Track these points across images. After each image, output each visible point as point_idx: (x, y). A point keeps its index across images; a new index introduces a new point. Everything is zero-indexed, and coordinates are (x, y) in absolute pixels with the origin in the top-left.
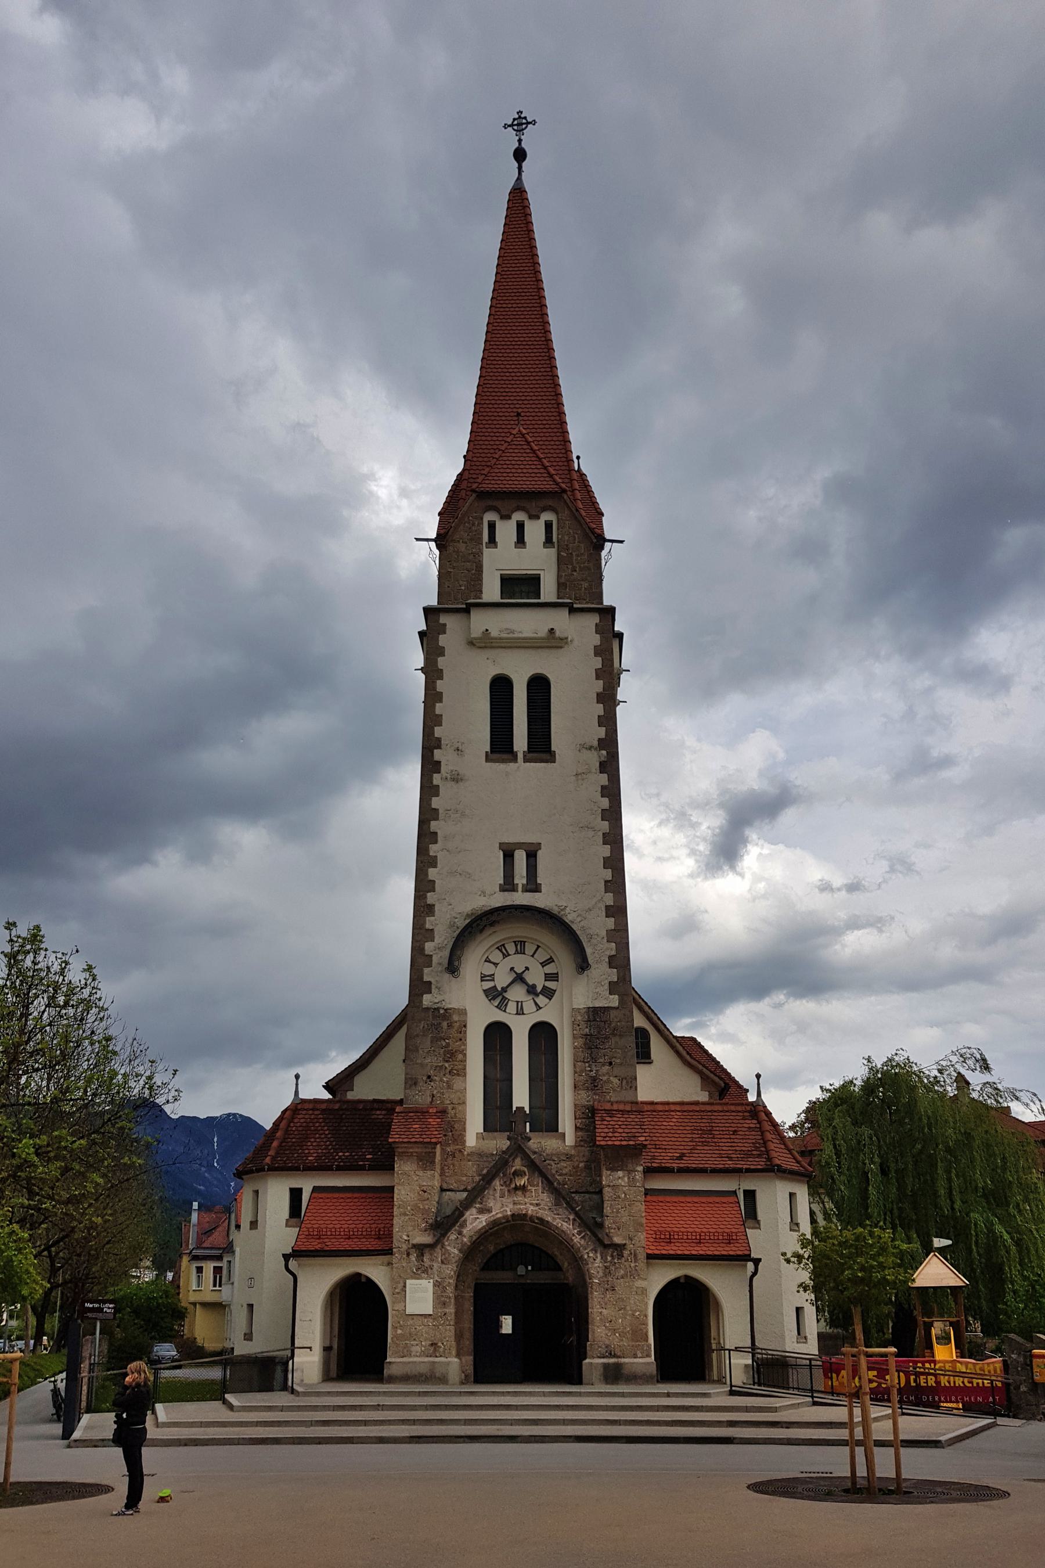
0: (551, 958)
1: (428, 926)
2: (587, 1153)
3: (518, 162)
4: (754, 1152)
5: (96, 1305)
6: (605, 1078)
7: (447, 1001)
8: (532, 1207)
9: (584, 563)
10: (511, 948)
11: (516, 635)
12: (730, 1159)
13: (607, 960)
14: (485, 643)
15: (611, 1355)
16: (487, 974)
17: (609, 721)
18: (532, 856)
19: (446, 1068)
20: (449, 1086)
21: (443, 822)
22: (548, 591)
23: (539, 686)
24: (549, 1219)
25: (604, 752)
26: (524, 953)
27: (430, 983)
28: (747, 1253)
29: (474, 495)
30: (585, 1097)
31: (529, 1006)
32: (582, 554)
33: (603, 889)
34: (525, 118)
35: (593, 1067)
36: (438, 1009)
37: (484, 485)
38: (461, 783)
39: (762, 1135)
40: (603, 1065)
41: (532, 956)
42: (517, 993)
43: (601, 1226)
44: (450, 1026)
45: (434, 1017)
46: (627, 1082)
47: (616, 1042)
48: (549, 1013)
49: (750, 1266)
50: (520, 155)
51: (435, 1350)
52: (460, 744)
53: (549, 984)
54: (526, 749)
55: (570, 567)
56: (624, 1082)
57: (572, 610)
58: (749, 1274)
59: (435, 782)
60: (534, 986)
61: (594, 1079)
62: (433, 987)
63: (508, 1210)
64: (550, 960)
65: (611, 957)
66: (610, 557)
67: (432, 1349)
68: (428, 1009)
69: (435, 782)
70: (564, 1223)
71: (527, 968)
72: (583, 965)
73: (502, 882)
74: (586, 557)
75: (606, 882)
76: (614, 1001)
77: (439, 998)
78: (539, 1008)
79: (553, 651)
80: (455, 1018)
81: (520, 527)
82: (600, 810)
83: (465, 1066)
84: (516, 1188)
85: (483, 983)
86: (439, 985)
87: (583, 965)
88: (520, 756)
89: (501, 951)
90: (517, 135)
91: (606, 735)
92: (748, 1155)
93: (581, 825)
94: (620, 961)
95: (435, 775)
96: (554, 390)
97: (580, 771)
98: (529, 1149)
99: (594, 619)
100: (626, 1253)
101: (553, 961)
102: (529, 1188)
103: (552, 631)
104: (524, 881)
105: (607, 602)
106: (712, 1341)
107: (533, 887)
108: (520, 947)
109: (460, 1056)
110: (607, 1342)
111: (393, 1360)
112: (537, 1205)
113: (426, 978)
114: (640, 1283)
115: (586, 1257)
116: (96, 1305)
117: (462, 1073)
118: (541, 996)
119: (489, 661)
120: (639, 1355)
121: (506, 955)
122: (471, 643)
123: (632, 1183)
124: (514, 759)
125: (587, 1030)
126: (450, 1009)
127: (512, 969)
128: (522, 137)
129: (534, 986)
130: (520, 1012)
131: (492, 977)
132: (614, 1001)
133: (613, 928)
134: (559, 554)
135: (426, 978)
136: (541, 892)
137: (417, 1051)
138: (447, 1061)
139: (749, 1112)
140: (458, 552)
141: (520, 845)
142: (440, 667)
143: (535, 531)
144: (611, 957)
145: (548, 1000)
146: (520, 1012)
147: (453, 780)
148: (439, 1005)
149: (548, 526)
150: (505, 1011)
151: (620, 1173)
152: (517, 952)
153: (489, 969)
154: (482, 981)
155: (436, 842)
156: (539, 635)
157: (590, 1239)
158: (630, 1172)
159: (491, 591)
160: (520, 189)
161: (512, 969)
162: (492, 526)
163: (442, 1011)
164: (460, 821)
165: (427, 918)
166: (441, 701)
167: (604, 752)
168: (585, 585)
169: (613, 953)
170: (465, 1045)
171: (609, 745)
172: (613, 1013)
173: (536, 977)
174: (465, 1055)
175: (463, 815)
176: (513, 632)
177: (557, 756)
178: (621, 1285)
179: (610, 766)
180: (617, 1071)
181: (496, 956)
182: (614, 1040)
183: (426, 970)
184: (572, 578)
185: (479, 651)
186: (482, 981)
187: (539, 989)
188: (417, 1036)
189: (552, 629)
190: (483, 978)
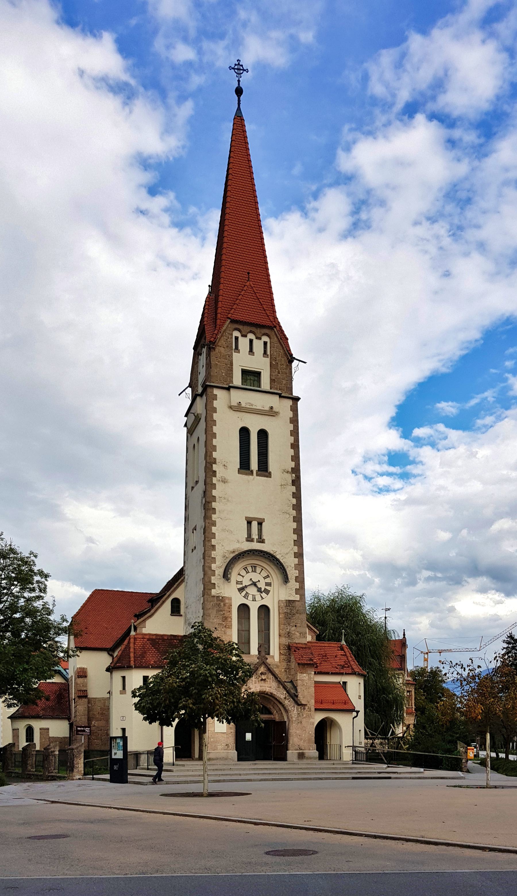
0: (268, 575)
1: (213, 556)
2: (286, 665)
3: (238, 96)
4: (346, 666)
5: (82, 729)
6: (293, 632)
7: (223, 593)
8: (268, 688)
9: (284, 370)
10: (250, 569)
11: (254, 407)
12: (337, 668)
13: (295, 578)
14: (238, 408)
15: (300, 749)
16: (239, 581)
17: (296, 458)
18: (260, 524)
19: (223, 625)
20: (225, 633)
21: (218, 503)
22: (265, 383)
23: (263, 435)
24: (275, 693)
25: (294, 475)
26: (256, 572)
27: (214, 584)
28: (354, 708)
29: (229, 320)
30: (285, 641)
31: (258, 597)
32: (283, 364)
33: (293, 544)
34: (242, 66)
35: (288, 627)
36: (219, 597)
37: (234, 316)
38: (226, 483)
39: (347, 658)
40: (293, 627)
41: (260, 574)
42: (252, 590)
43: (297, 696)
44: (224, 605)
45: (218, 600)
46: (303, 635)
47: (298, 617)
48: (268, 601)
49: (354, 714)
50: (239, 91)
51: (228, 747)
52: (225, 463)
53: (267, 587)
54: (257, 469)
55: (277, 371)
56: (301, 634)
57: (281, 396)
58: (353, 716)
59: (214, 482)
60: (261, 588)
61: (289, 633)
62: (216, 586)
63: (258, 689)
64: (268, 576)
65: (296, 577)
66: (297, 369)
67: (226, 747)
68: (214, 596)
69: (214, 482)
70: (281, 694)
71: (259, 581)
72: (286, 580)
73: (247, 537)
74: (285, 366)
75: (295, 541)
76: (297, 597)
77: (219, 592)
78: (262, 598)
79: (270, 417)
80: (227, 601)
81: (251, 341)
82: (292, 505)
83: (232, 624)
84: (262, 680)
85: (237, 585)
86: (219, 585)
87: (286, 580)
88: (255, 472)
89: (245, 570)
90: (237, 77)
91: (295, 466)
92: (343, 667)
93: (283, 511)
94: (300, 579)
95: (214, 478)
96: (264, 259)
97: (283, 484)
98: (267, 663)
99: (290, 402)
100: (306, 708)
101: (269, 577)
102: (267, 680)
103: (272, 408)
104: (257, 537)
105: (295, 394)
106: (328, 744)
107: (261, 540)
108: (254, 568)
109: (229, 619)
110: (298, 744)
111: (210, 752)
112: (270, 687)
113: (213, 582)
114: (312, 720)
115: (290, 709)
116: (82, 729)
117: (230, 627)
118: (263, 593)
119: (239, 419)
120: (311, 749)
121: (248, 572)
122: (231, 407)
123: (310, 679)
124: (252, 473)
125: (286, 610)
126: (225, 597)
127: (251, 579)
128: (240, 79)
129: (261, 588)
130: (254, 600)
131: (241, 583)
132: (297, 597)
133: (297, 563)
134: (271, 363)
135: (213, 582)
136: (265, 543)
137: (210, 616)
138: (224, 621)
139: (340, 647)
140: (220, 353)
141: (255, 519)
142: (214, 419)
143: (258, 345)
144: (296, 577)
145: (266, 595)
146: (254, 600)
147: (222, 481)
148: (219, 595)
149: (265, 343)
150: (247, 599)
151: (305, 675)
152: (252, 571)
153: (240, 579)
154: (237, 584)
155: (215, 514)
156: (265, 409)
157: (292, 701)
158: (309, 674)
159: (237, 380)
160: (240, 117)
161: (251, 579)
162: (237, 338)
163: (221, 598)
164: (226, 504)
165: (212, 552)
166: (215, 438)
167: (294, 475)
168: (284, 382)
169: (297, 575)
170: (231, 614)
171: (296, 470)
172: (297, 603)
173: (262, 585)
174: (231, 619)
175: (228, 501)
176: (252, 405)
177: (272, 474)
178: (304, 721)
179: (296, 482)
180: (298, 629)
181: (243, 573)
182: (297, 615)
183: (212, 578)
184: (278, 377)
185: (234, 412)
186: (237, 584)
187: (263, 590)
188: (210, 609)
189: (272, 407)
190: (238, 583)
